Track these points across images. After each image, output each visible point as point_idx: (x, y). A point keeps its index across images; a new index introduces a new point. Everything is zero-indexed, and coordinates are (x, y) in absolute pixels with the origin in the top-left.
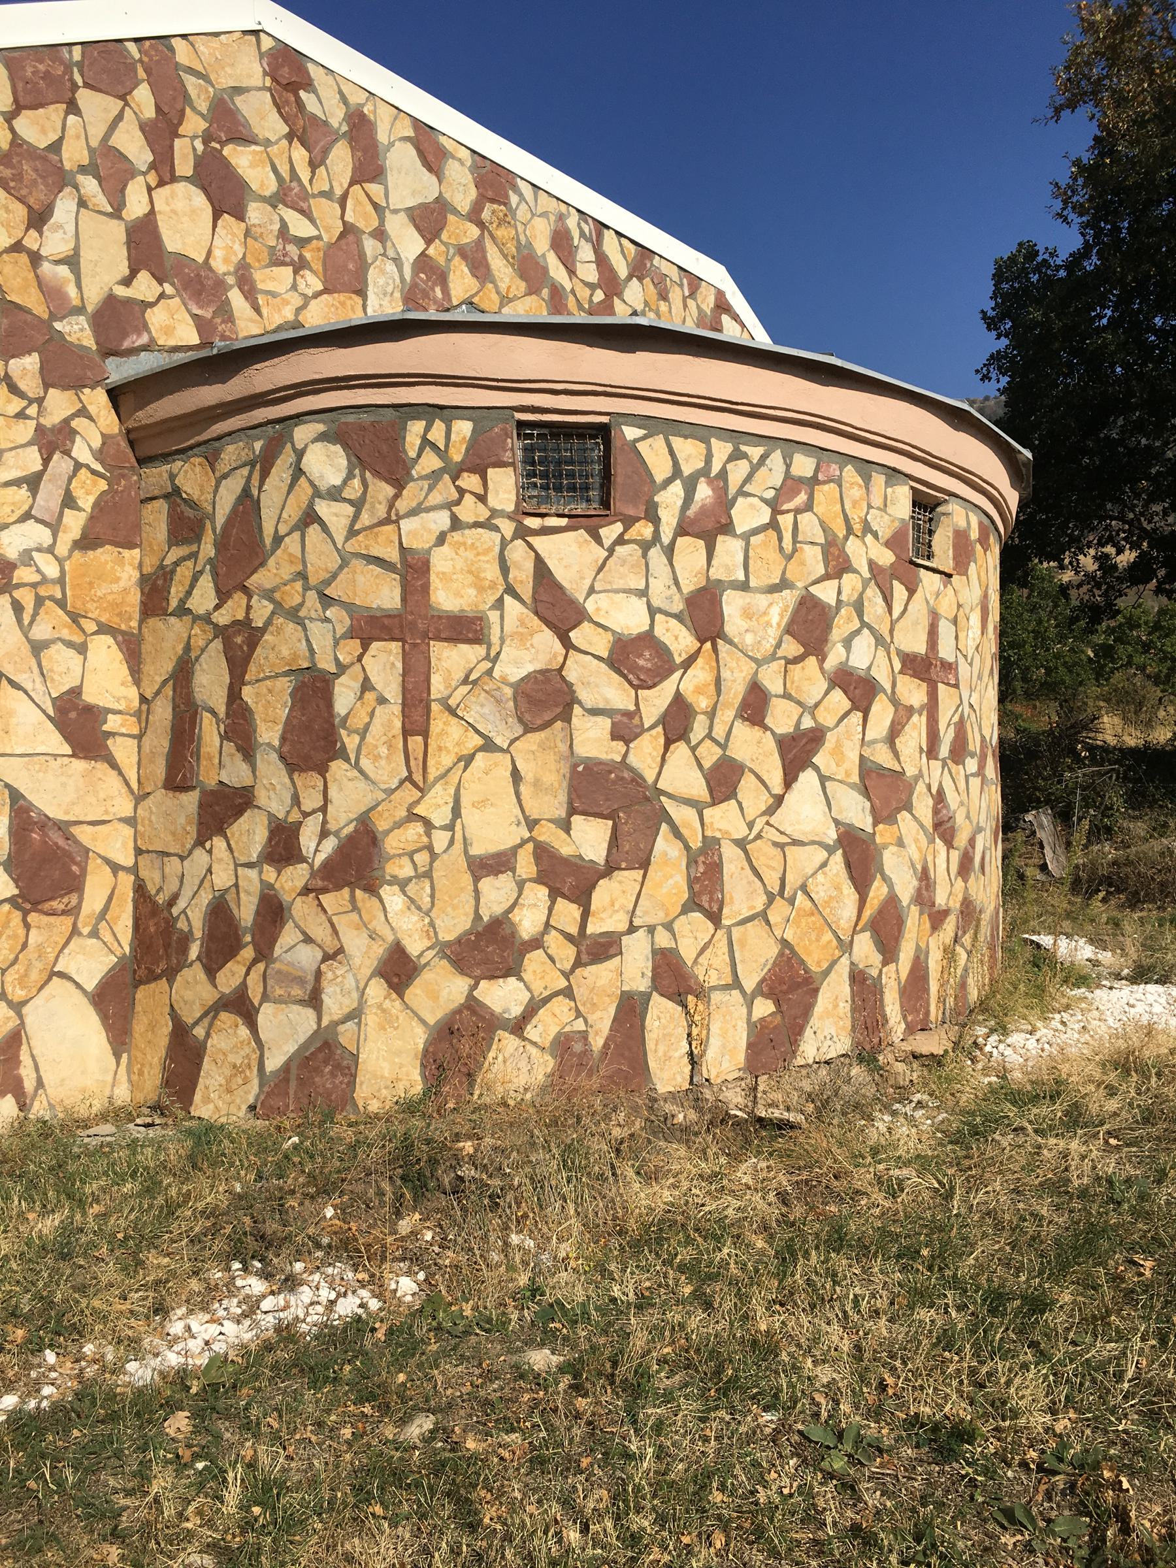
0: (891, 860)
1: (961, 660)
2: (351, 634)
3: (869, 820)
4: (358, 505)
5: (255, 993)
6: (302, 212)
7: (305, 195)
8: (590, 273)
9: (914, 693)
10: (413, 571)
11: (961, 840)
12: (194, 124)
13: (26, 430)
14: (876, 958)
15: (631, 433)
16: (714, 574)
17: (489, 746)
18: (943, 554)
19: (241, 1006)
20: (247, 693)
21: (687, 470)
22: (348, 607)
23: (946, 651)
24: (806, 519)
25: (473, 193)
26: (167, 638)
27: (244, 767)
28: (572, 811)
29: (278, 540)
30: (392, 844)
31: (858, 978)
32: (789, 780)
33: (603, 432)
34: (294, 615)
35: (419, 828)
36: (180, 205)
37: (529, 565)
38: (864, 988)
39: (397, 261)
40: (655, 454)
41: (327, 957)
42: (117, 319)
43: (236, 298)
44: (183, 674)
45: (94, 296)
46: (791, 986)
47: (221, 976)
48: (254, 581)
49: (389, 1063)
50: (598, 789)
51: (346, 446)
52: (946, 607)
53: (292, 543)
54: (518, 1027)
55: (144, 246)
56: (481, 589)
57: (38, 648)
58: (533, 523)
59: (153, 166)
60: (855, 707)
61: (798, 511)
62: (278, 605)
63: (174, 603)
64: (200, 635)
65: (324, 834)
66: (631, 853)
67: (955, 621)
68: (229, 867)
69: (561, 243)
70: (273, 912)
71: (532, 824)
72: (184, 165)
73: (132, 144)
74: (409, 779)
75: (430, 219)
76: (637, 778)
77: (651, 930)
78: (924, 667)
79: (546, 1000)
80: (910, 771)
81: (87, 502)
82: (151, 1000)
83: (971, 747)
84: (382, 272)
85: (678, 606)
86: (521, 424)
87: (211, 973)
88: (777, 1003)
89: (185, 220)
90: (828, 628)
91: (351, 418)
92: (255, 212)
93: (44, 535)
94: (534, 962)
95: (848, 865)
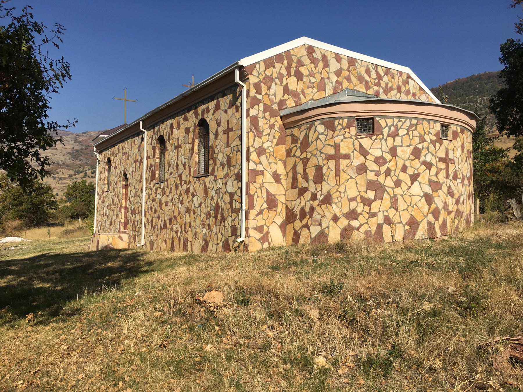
0: (436, 199)
1: (455, 158)
2: (326, 159)
3: (431, 191)
4: (327, 135)
5: (309, 224)
6: (313, 77)
7: (314, 74)
8: (374, 76)
9: (442, 165)
10: (337, 147)
11: (456, 196)
12: (294, 65)
13: (267, 126)
14: (433, 219)
15: (377, 119)
16: (395, 144)
17: (351, 178)
18: (450, 137)
19: (307, 226)
20: (307, 170)
21: (389, 125)
22: (325, 154)
23: (451, 156)
24: (415, 132)
25: (348, 65)
26: (291, 161)
27: (306, 184)
28: (367, 189)
29: (312, 142)
30: (334, 196)
31: (429, 223)
32: (412, 183)
33: (372, 119)
34: (315, 156)
35: (339, 193)
36: (292, 81)
37: (358, 145)
38: (431, 226)
39: (332, 83)
40: (382, 122)
41: (322, 217)
42: (282, 104)
43: (302, 96)
44: (294, 167)
45: (278, 100)
46: (413, 224)
47: (303, 221)
48: (307, 150)
49: (334, 236)
50: (371, 185)
51: (324, 125)
52: (451, 146)
53: (315, 143)
54: (358, 229)
55: (286, 90)
56: (349, 149)
57: (270, 164)
58: (359, 137)
59: (287, 74)
60: (427, 169)
61: (413, 130)
62: (312, 154)
63: (292, 155)
64: (298, 160)
65: (321, 195)
66: (379, 197)
67: (453, 150)
68: (305, 202)
69: (368, 71)
70: (312, 209)
71: (360, 192)
72: (292, 73)
73: (284, 72)
74: (337, 184)
75: (338, 73)
76: (380, 183)
77: (383, 211)
78: (445, 160)
79: (363, 224)
80: (441, 182)
81: (277, 137)
82: (290, 227)
83: (459, 177)
84: (329, 85)
85: (388, 150)
86: (356, 119)
87: (301, 221)
88: (410, 227)
89: (293, 84)
90: (421, 153)
91: (325, 120)
92: (305, 79)
93: (270, 144)
94: (360, 217)
95: (426, 200)
